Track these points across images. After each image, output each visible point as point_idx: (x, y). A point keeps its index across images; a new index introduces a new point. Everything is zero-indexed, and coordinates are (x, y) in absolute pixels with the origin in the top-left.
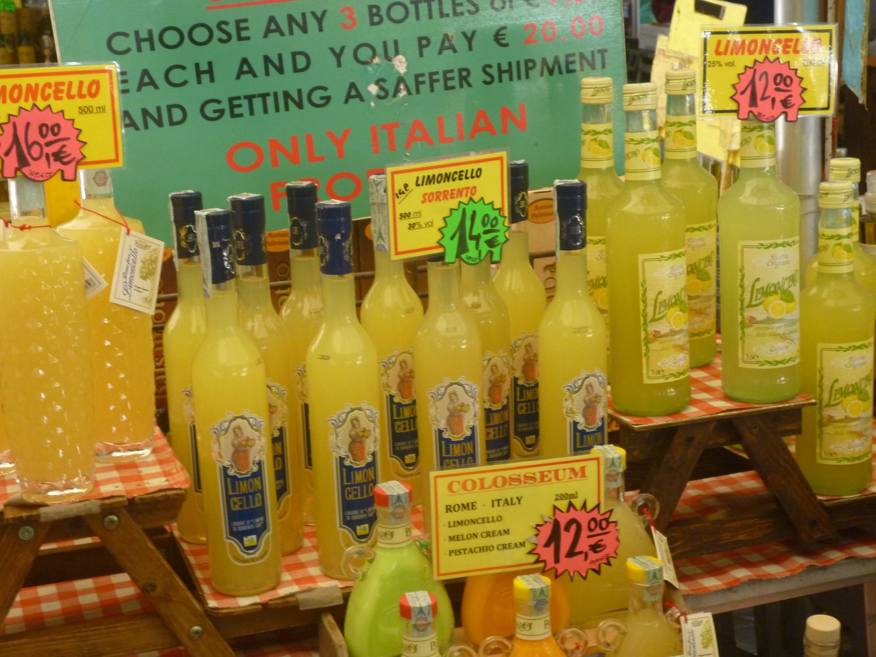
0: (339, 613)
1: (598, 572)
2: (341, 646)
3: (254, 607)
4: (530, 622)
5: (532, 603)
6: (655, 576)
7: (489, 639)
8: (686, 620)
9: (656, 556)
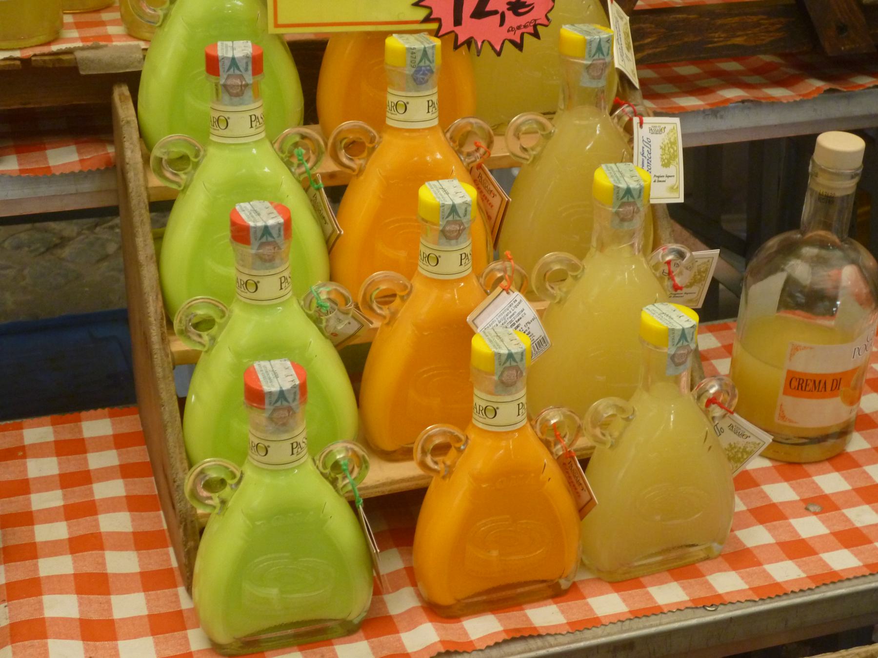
0: (133, 80)
1: (519, 46)
2: (128, 122)
3: (8, 62)
4: (405, 100)
5: (409, 71)
6: (599, 49)
7: (346, 124)
8: (641, 123)
9: (609, 26)
